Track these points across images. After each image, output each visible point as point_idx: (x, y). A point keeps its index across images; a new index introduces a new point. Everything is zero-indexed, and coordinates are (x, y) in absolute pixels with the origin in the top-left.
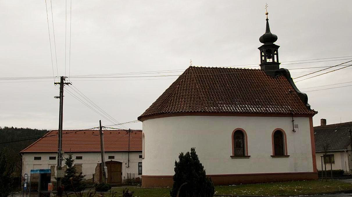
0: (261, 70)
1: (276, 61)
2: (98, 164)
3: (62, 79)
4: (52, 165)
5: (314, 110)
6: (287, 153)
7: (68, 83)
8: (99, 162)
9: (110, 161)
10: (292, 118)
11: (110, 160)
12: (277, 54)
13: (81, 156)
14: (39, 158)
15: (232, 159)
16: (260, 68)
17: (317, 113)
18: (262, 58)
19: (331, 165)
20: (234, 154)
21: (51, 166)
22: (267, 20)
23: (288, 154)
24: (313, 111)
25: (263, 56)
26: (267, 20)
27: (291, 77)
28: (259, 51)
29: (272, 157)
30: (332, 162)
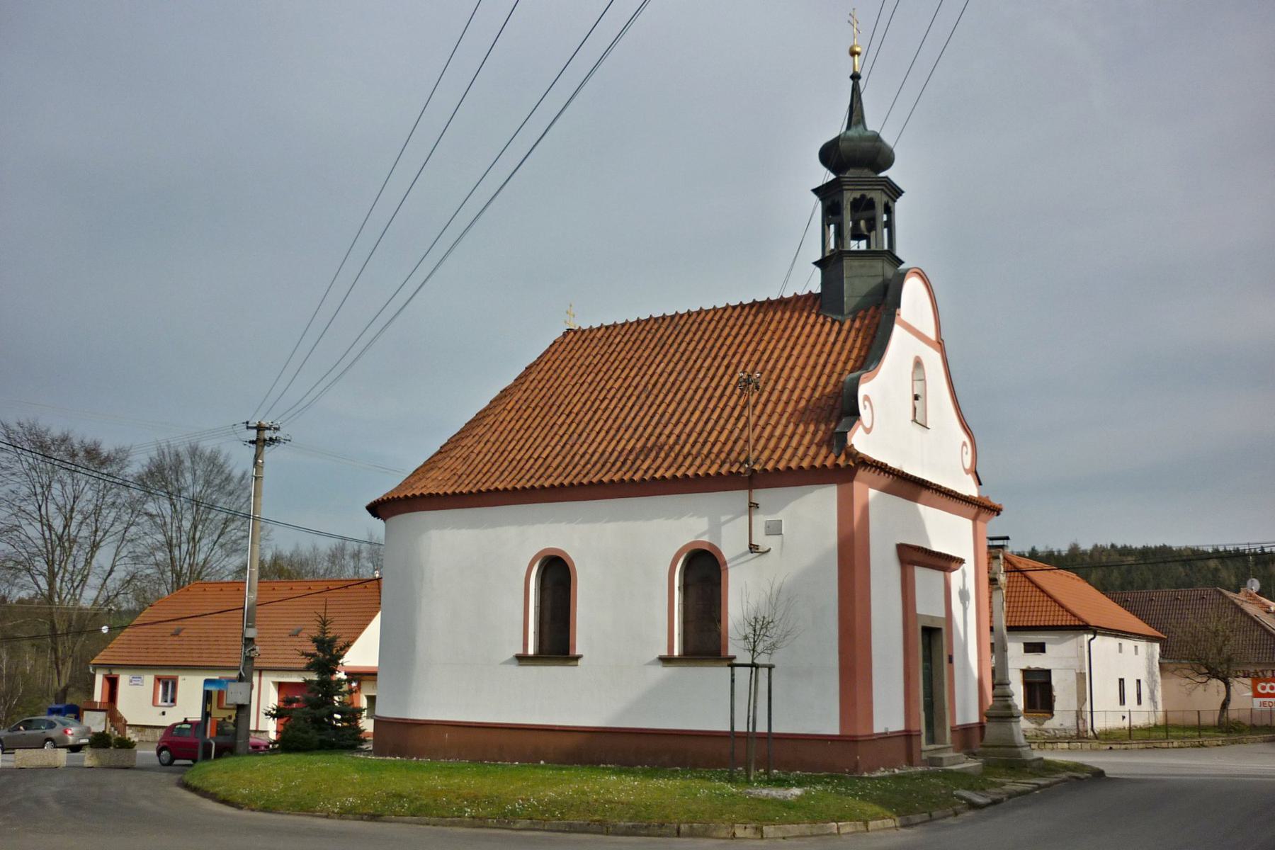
12: (889, 225)
22: (855, 77)
26: (855, 77)
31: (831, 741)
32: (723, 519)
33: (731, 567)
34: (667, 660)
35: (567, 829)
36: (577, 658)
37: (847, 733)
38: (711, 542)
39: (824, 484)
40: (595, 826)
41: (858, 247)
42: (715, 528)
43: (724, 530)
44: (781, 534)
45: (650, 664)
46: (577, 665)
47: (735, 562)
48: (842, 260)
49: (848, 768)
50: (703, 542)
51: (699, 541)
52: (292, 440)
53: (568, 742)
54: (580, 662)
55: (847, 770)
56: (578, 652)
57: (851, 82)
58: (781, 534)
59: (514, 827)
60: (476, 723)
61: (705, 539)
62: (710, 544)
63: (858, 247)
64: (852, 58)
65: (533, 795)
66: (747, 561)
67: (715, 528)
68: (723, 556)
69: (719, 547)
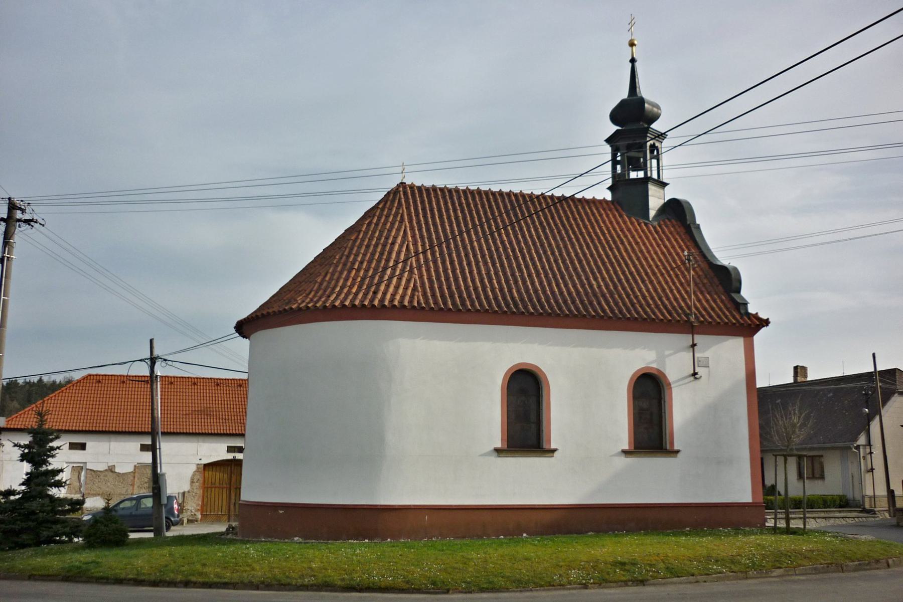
0: (612, 202)
1: (649, 175)
2: (198, 464)
3: (12, 206)
4: (75, 465)
5: (757, 313)
6: (672, 444)
7: (32, 220)
8: (200, 459)
9: (232, 458)
10: (691, 335)
11: (230, 456)
13: (84, 442)
14: (82, 447)
15: (498, 456)
16: (608, 196)
17: (766, 322)
18: (616, 168)
19: (776, 462)
20: (506, 443)
21: (73, 467)
22: (633, 61)
23: (676, 448)
24: (756, 316)
25: (619, 162)
26: (633, 61)
27: (698, 222)
28: (608, 149)
29: (624, 455)
30: (818, 475)
31: (748, 506)
32: (667, 353)
33: (674, 387)
34: (626, 453)
35: (813, 572)
36: (554, 451)
37: (755, 501)
38: (658, 368)
39: (734, 335)
40: (833, 567)
41: (637, 176)
42: (661, 358)
43: (667, 361)
44: (709, 367)
45: (617, 455)
46: (553, 457)
47: (677, 384)
48: (648, 183)
49: (759, 524)
50: (652, 368)
51: (650, 367)
52: (45, 226)
53: (548, 517)
54: (556, 454)
55: (759, 525)
56: (553, 446)
57: (630, 65)
58: (709, 367)
59: (773, 575)
60: (455, 506)
61: (654, 365)
62: (658, 371)
63: (637, 176)
64: (630, 48)
65: (427, 560)
66: (680, 385)
67: (661, 358)
68: (668, 379)
69: (664, 372)
